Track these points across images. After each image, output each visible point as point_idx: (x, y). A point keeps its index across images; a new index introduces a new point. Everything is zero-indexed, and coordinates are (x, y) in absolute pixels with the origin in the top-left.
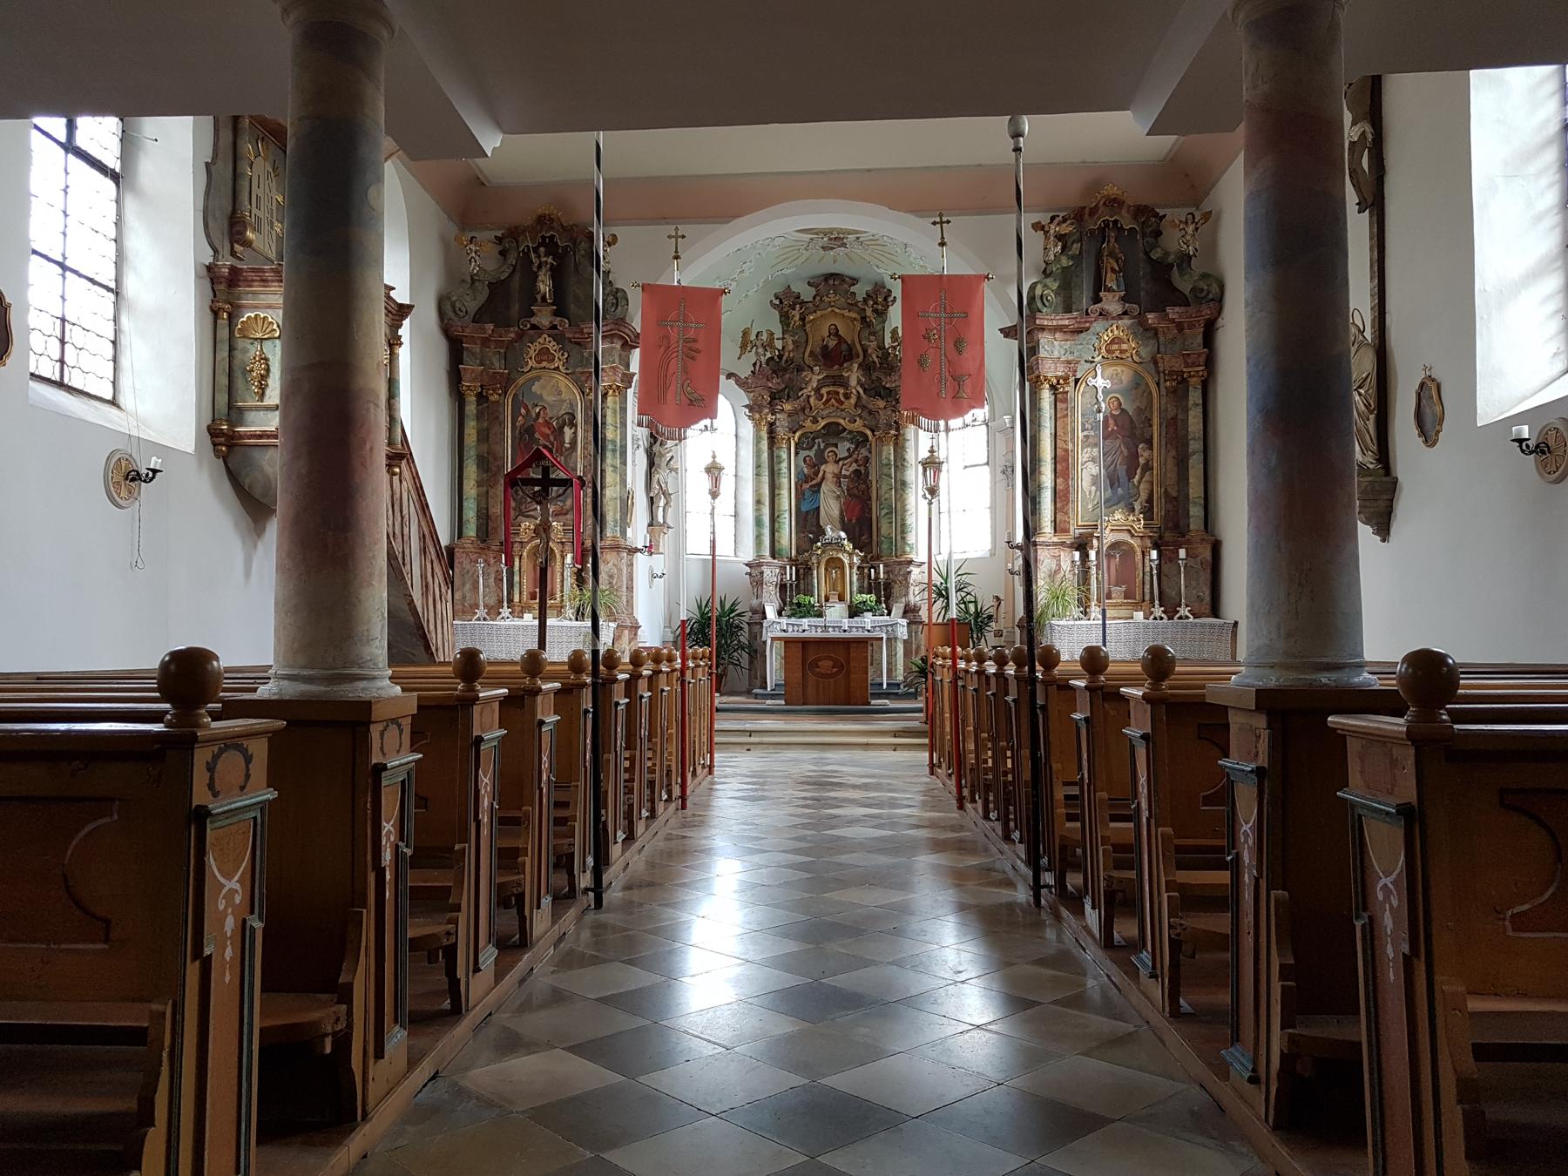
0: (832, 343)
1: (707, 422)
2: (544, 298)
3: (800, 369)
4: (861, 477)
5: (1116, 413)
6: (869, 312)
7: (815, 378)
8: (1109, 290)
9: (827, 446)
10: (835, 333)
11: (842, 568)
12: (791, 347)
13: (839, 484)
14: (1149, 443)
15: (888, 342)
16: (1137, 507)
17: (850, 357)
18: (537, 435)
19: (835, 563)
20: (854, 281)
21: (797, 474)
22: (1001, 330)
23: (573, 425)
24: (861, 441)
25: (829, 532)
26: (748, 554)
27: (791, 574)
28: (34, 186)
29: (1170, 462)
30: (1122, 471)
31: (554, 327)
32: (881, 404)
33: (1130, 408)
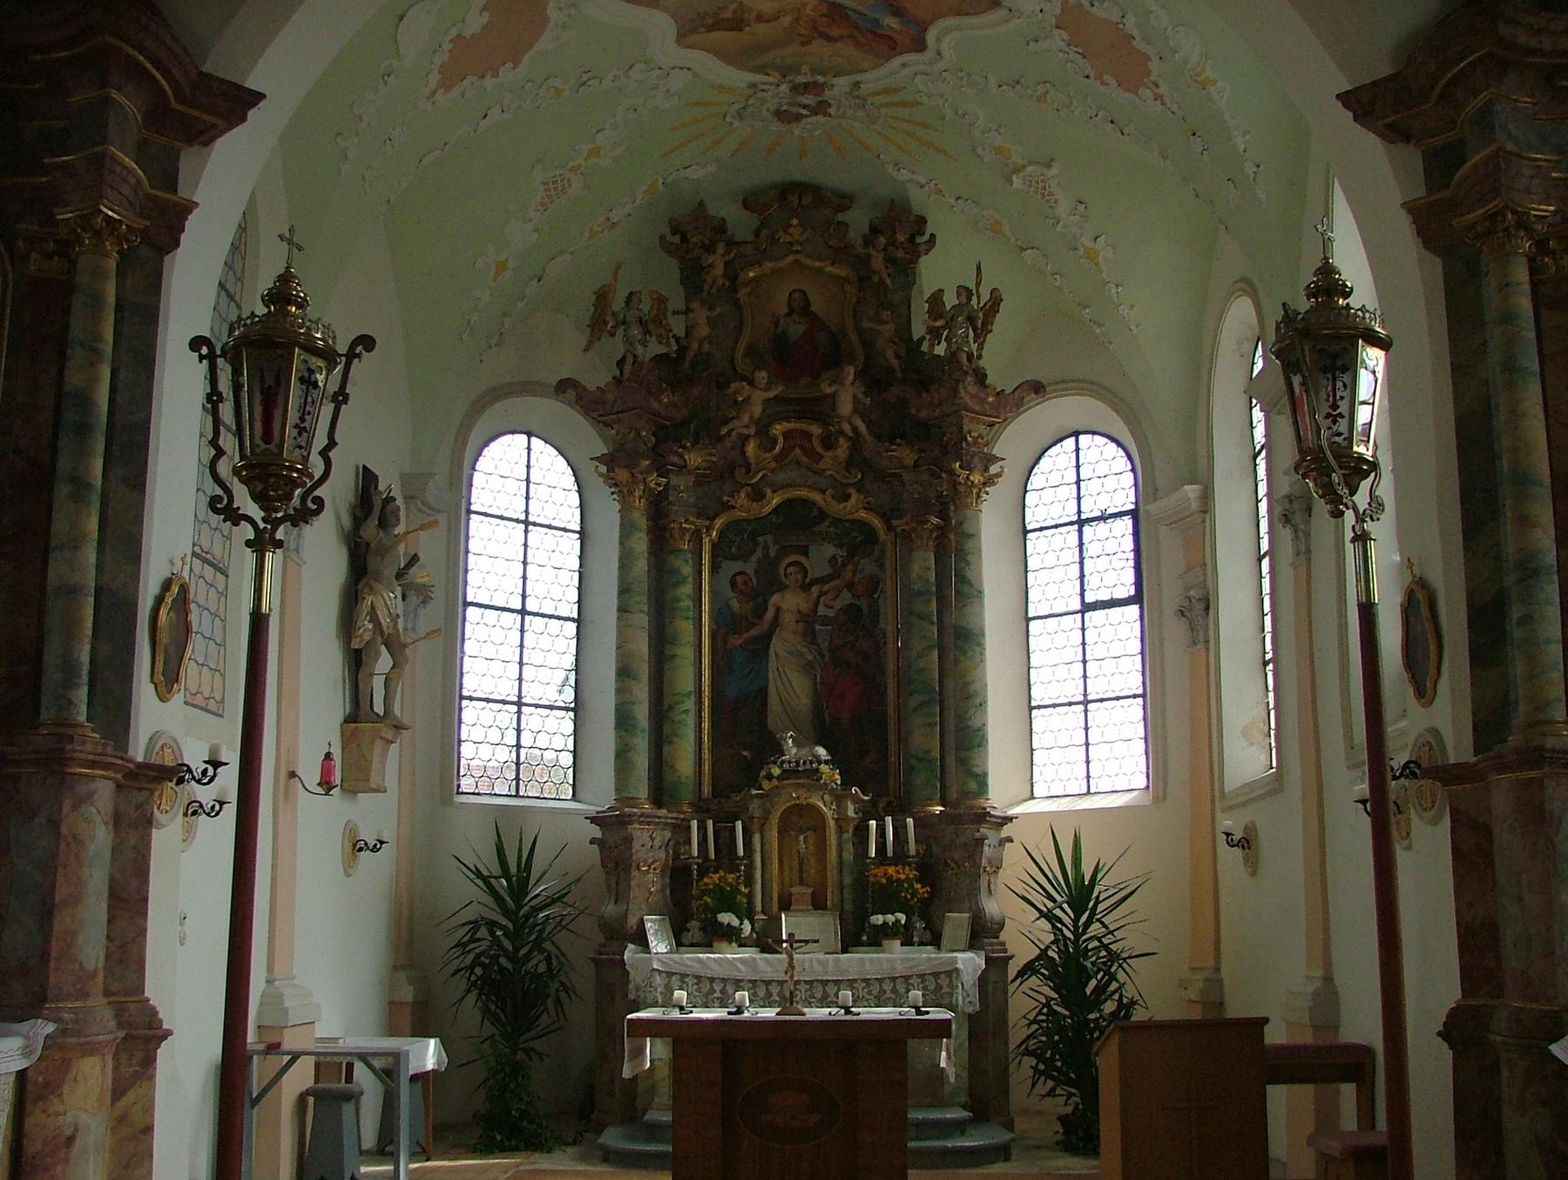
0: (796, 329)
6: (878, 262)
7: (757, 397)
9: (785, 550)
10: (799, 305)
11: (819, 827)
12: (704, 331)
13: (810, 635)
15: (918, 330)
17: (835, 359)
20: (844, 201)
21: (717, 614)
25: (791, 750)
26: (603, 797)
32: (908, 455)
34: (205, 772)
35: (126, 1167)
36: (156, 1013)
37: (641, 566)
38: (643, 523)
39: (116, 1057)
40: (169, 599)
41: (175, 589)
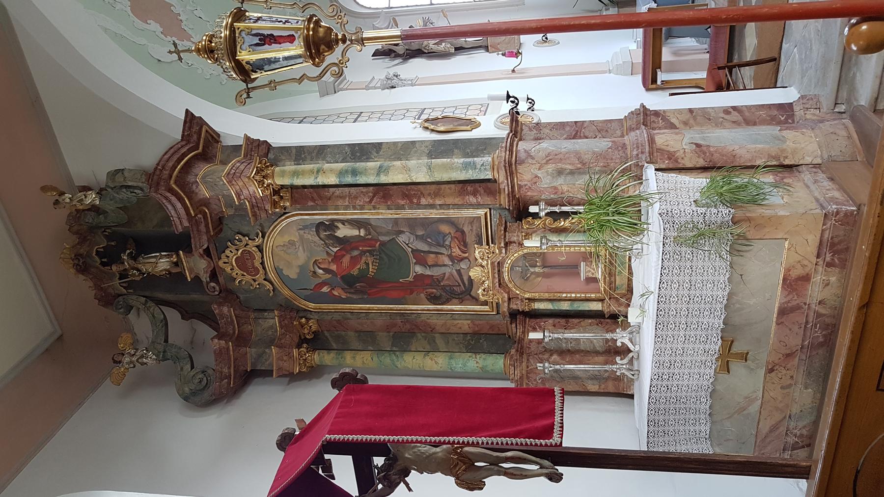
2: (176, 264)
18: (355, 272)
23: (331, 226)
28: (487, 21)
31: (207, 252)
34: (512, 102)
35: (710, 119)
36: (632, 112)
39: (654, 129)
40: (432, 127)
41: (426, 125)
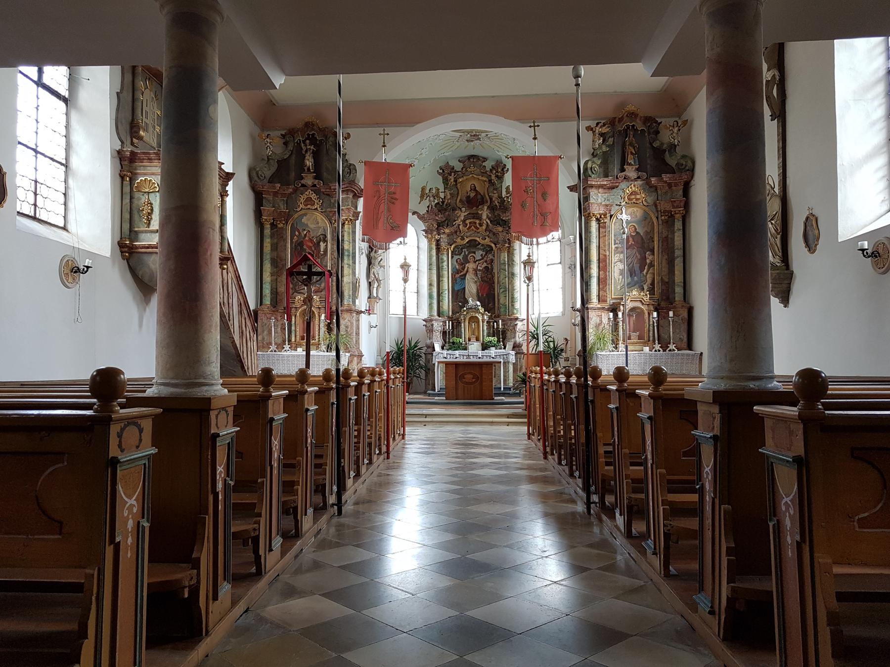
0: (472, 195)
1: (401, 239)
2: (309, 169)
3: (454, 210)
4: (488, 271)
5: (633, 234)
6: (493, 177)
7: (462, 214)
8: (630, 164)
9: (469, 253)
10: (474, 189)
11: (478, 322)
12: (449, 197)
13: (476, 275)
14: (652, 251)
15: (504, 194)
16: (646, 287)
17: (482, 202)
18: (305, 247)
19: (474, 320)
20: (485, 159)
21: (452, 269)
22: (568, 187)
23: (325, 241)
24: (488, 250)
25: (471, 302)
26: (425, 314)
27: (449, 326)
29: (664, 262)
30: (637, 267)
31: (314, 186)
32: (500, 229)
33: (641, 232)
37: (434, 258)
38: (434, 247)
